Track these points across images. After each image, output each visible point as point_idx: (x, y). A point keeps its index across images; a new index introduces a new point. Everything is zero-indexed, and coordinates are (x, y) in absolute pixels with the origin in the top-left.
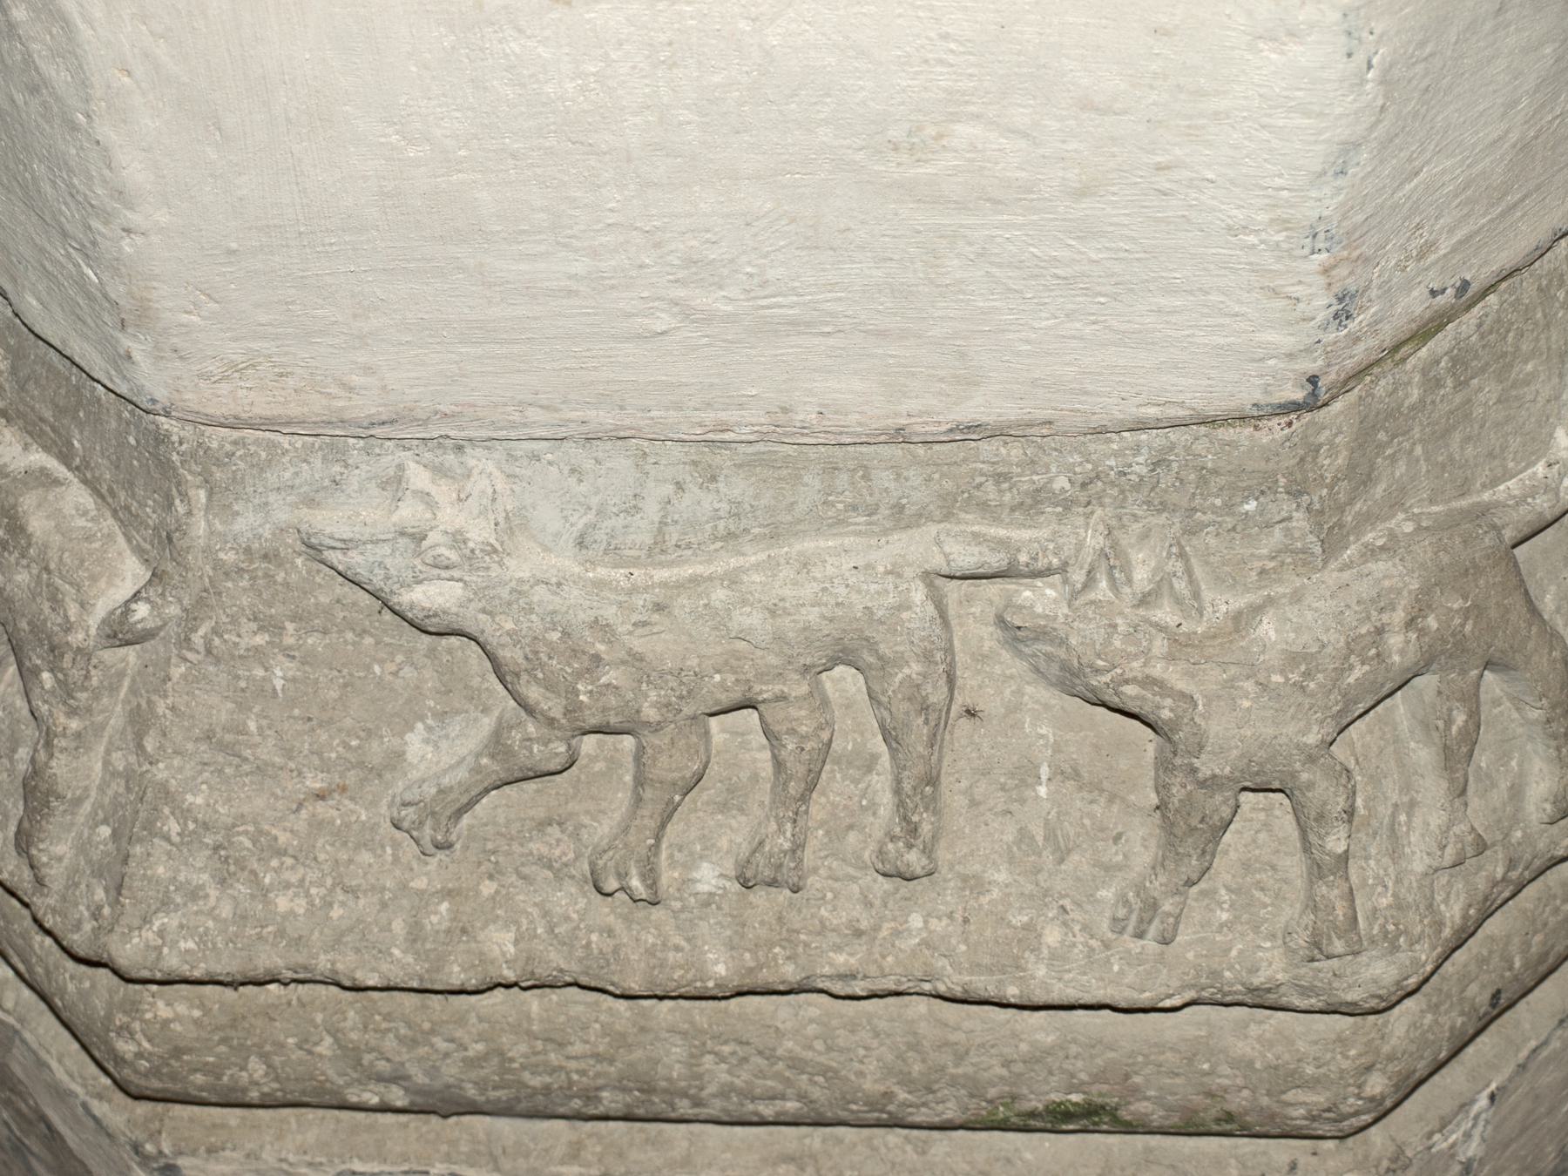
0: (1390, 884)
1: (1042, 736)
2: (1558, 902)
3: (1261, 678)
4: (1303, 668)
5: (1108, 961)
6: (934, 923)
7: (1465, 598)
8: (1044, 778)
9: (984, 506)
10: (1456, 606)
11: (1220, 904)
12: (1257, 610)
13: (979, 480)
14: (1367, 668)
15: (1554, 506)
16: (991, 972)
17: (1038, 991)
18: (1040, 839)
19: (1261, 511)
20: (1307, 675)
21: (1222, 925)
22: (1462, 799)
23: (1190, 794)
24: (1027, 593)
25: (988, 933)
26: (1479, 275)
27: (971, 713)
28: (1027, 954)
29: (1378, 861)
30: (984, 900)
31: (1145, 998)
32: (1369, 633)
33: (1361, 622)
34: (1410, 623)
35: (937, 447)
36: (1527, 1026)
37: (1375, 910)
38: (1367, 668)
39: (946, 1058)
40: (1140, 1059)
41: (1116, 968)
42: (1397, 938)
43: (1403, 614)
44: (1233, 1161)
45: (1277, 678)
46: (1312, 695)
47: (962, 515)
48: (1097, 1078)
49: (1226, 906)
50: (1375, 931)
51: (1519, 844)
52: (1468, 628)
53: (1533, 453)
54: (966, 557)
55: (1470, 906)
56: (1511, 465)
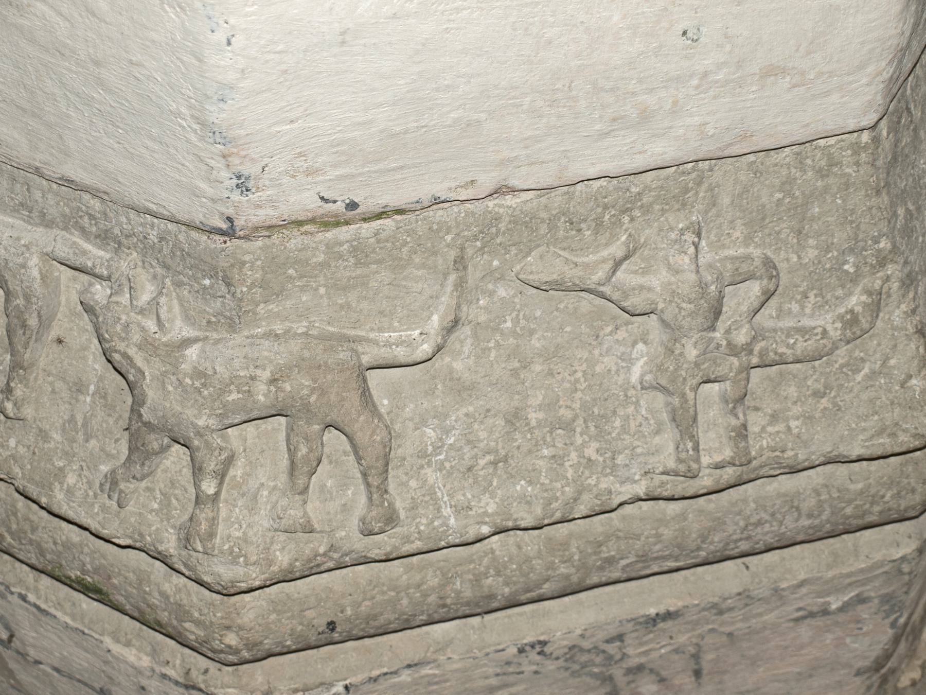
0: (244, 526)
1: (95, 369)
2: (385, 588)
3: (180, 376)
4: (203, 380)
5: (92, 505)
6: (20, 448)
7: (315, 381)
8: (91, 392)
9: (83, 230)
10: (307, 383)
11: (155, 498)
12: (196, 340)
13: (81, 214)
14: (240, 396)
15: (408, 356)
16: (37, 486)
17: (55, 506)
18: (80, 424)
19: (212, 286)
20: (204, 385)
21: (152, 510)
22: (302, 497)
23: (139, 427)
24: (98, 287)
25: (42, 464)
26: (369, 202)
27: (60, 341)
28: (56, 484)
29: (241, 511)
30: (46, 446)
31: (105, 532)
32: (245, 376)
33: (243, 368)
34: (273, 381)
35: (63, 188)
36: (386, 659)
37: (229, 536)
38: (240, 396)
39: (27, 527)
40: (116, 570)
41: (96, 510)
42: (239, 557)
43: (270, 375)
44: (179, 655)
45: (188, 381)
46: (204, 398)
47: (73, 230)
48: (96, 571)
49: (158, 501)
50: (226, 547)
51: (341, 539)
52: (313, 399)
53: (414, 323)
54: (63, 251)
55: (296, 560)
56: (396, 324)
